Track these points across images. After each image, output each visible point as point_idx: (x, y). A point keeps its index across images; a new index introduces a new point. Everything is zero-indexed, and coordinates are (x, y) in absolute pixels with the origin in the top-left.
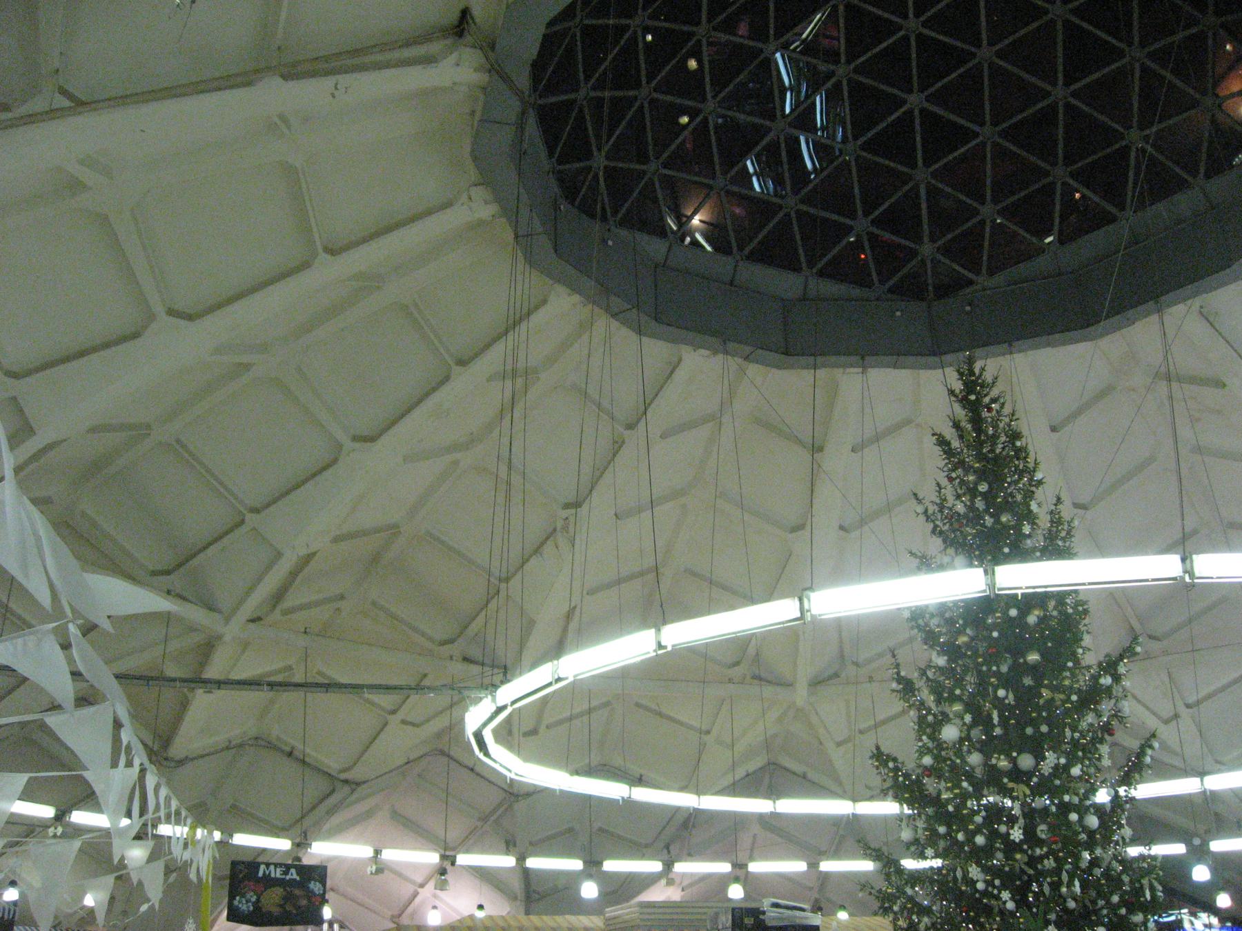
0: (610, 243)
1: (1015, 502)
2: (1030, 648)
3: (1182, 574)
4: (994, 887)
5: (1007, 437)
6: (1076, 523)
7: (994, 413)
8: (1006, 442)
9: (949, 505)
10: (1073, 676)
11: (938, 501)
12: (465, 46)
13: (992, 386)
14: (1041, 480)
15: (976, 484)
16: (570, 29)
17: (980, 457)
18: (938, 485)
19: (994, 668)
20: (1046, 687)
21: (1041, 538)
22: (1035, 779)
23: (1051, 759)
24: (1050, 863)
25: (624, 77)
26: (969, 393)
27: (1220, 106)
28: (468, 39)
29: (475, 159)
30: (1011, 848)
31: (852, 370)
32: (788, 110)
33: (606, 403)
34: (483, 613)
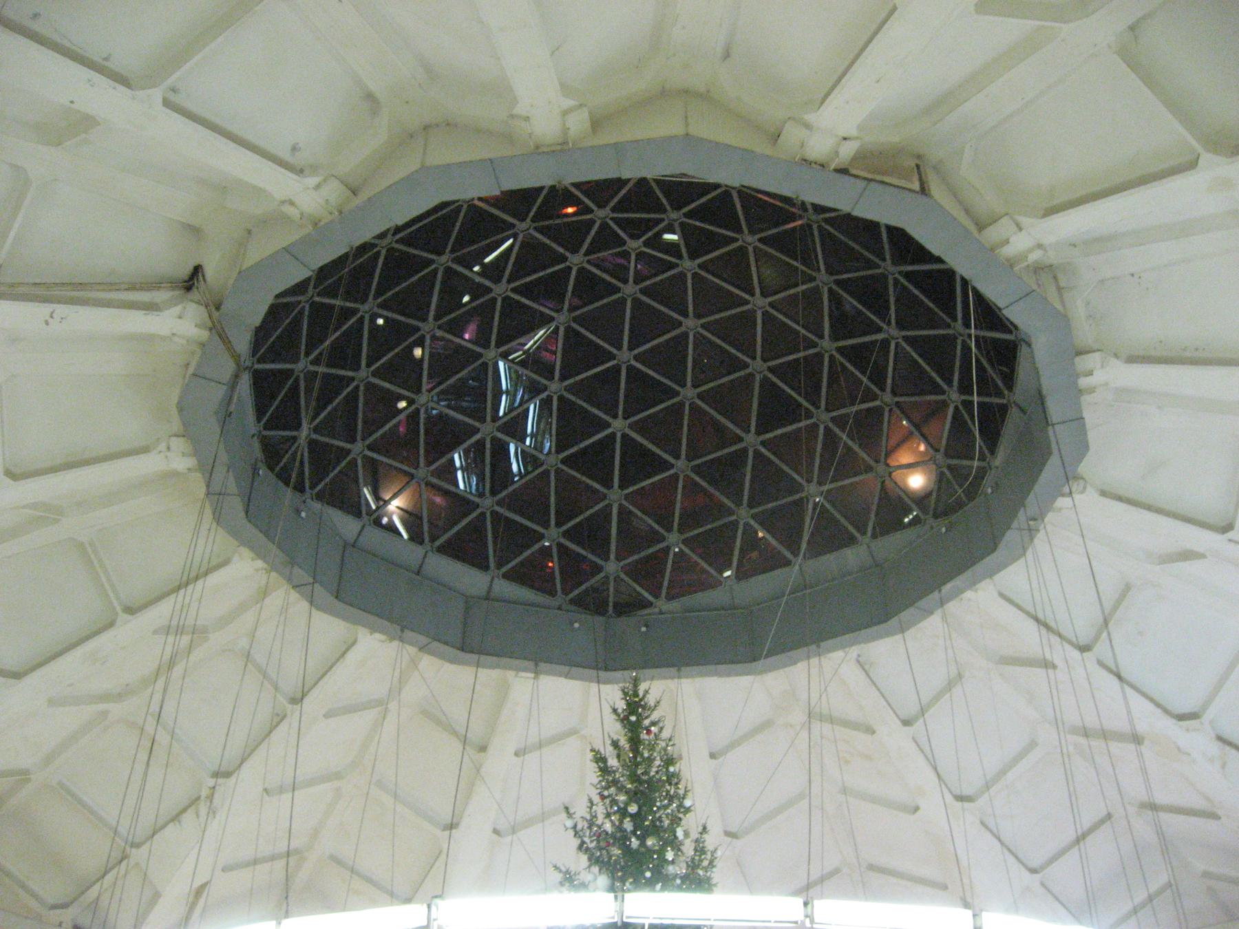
0: (303, 514)
1: (662, 827)
3: (803, 918)
5: (662, 761)
6: (719, 853)
7: (652, 736)
8: (660, 766)
9: (599, 822)
11: (588, 817)
12: (192, 301)
13: (653, 710)
14: (690, 807)
15: (627, 804)
16: (300, 302)
17: (634, 778)
18: (591, 801)
21: (685, 865)
25: (344, 355)
26: (631, 713)
27: (890, 473)
28: (195, 294)
29: (181, 409)
31: (523, 674)
32: (501, 413)
33: (272, 673)
34: (99, 884)
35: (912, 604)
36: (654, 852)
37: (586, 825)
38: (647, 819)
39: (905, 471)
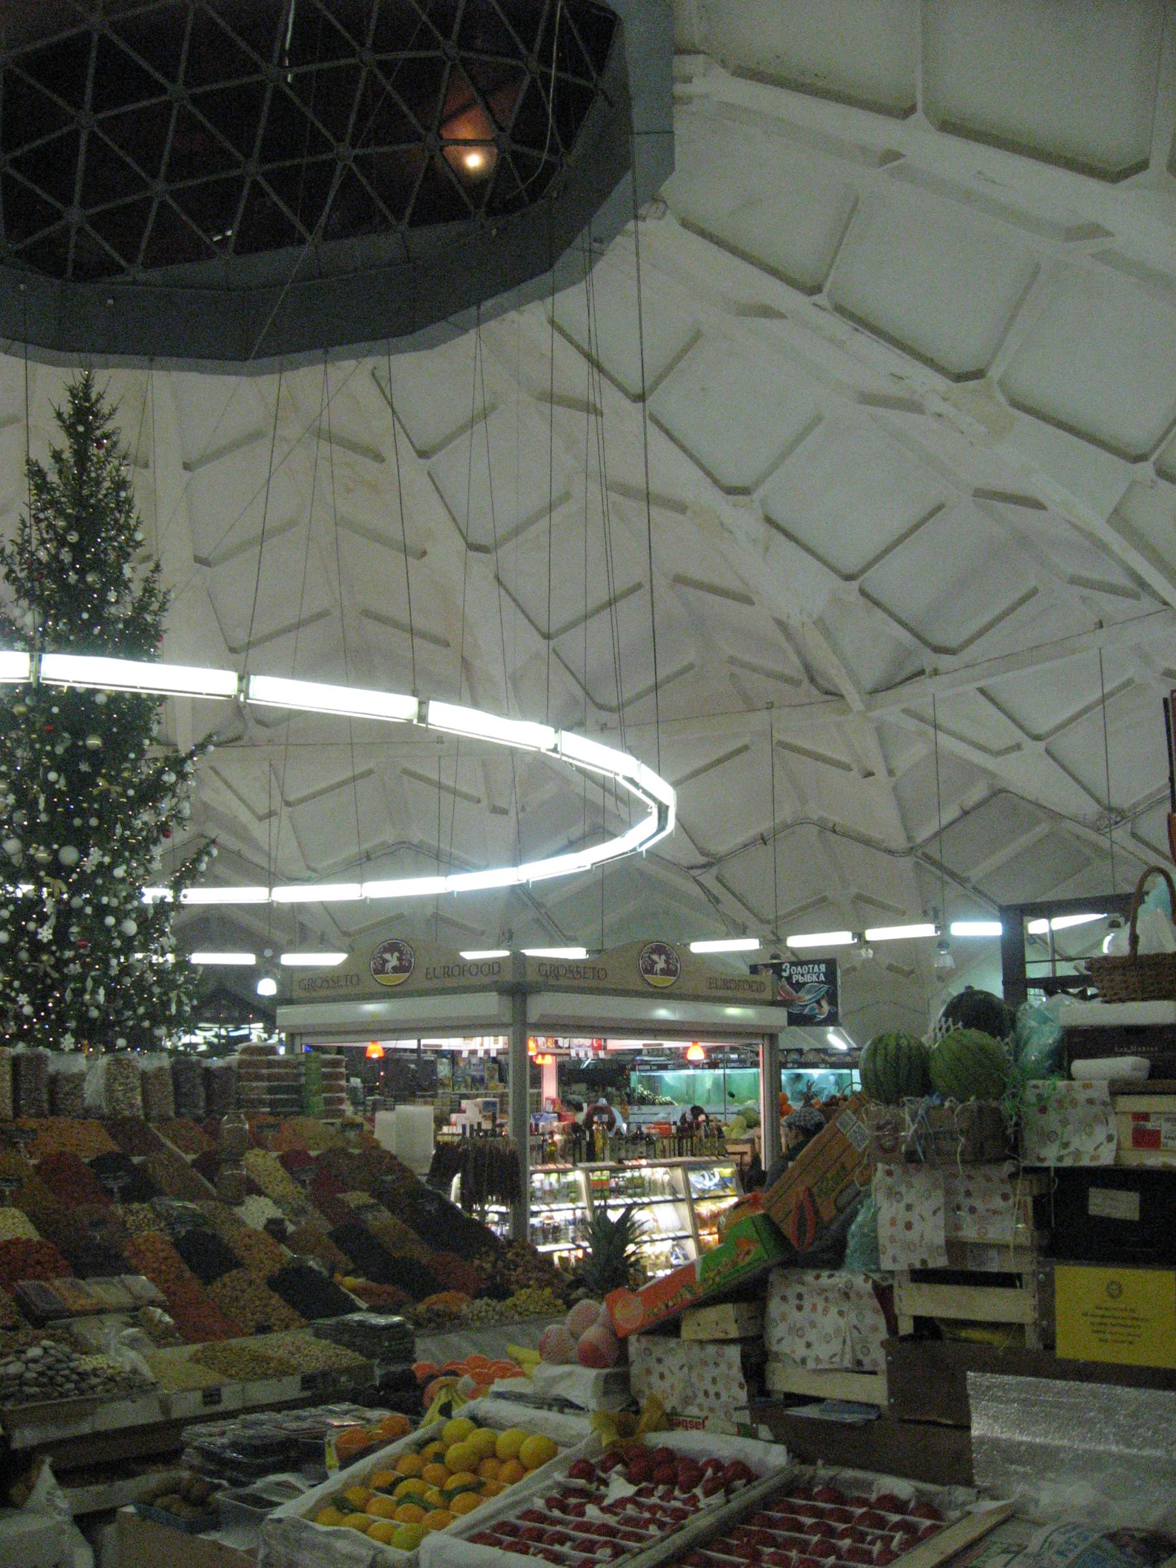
2: (94, 731)
4: (12, 989)
6: (173, 595)
8: (109, 488)
10: (134, 769)
11: (19, 541)
17: (80, 501)
18: (23, 522)
19: (48, 748)
20: (104, 776)
21: (130, 607)
22: (75, 876)
23: (95, 856)
24: (75, 968)
26: (80, 422)
30: (37, 948)
35: (444, 318)
36: (95, 591)
37: (16, 549)
38: (89, 552)
39: (460, 148)
